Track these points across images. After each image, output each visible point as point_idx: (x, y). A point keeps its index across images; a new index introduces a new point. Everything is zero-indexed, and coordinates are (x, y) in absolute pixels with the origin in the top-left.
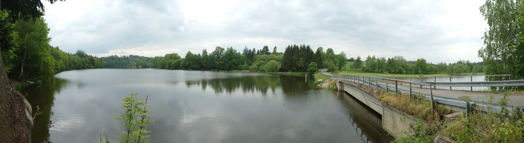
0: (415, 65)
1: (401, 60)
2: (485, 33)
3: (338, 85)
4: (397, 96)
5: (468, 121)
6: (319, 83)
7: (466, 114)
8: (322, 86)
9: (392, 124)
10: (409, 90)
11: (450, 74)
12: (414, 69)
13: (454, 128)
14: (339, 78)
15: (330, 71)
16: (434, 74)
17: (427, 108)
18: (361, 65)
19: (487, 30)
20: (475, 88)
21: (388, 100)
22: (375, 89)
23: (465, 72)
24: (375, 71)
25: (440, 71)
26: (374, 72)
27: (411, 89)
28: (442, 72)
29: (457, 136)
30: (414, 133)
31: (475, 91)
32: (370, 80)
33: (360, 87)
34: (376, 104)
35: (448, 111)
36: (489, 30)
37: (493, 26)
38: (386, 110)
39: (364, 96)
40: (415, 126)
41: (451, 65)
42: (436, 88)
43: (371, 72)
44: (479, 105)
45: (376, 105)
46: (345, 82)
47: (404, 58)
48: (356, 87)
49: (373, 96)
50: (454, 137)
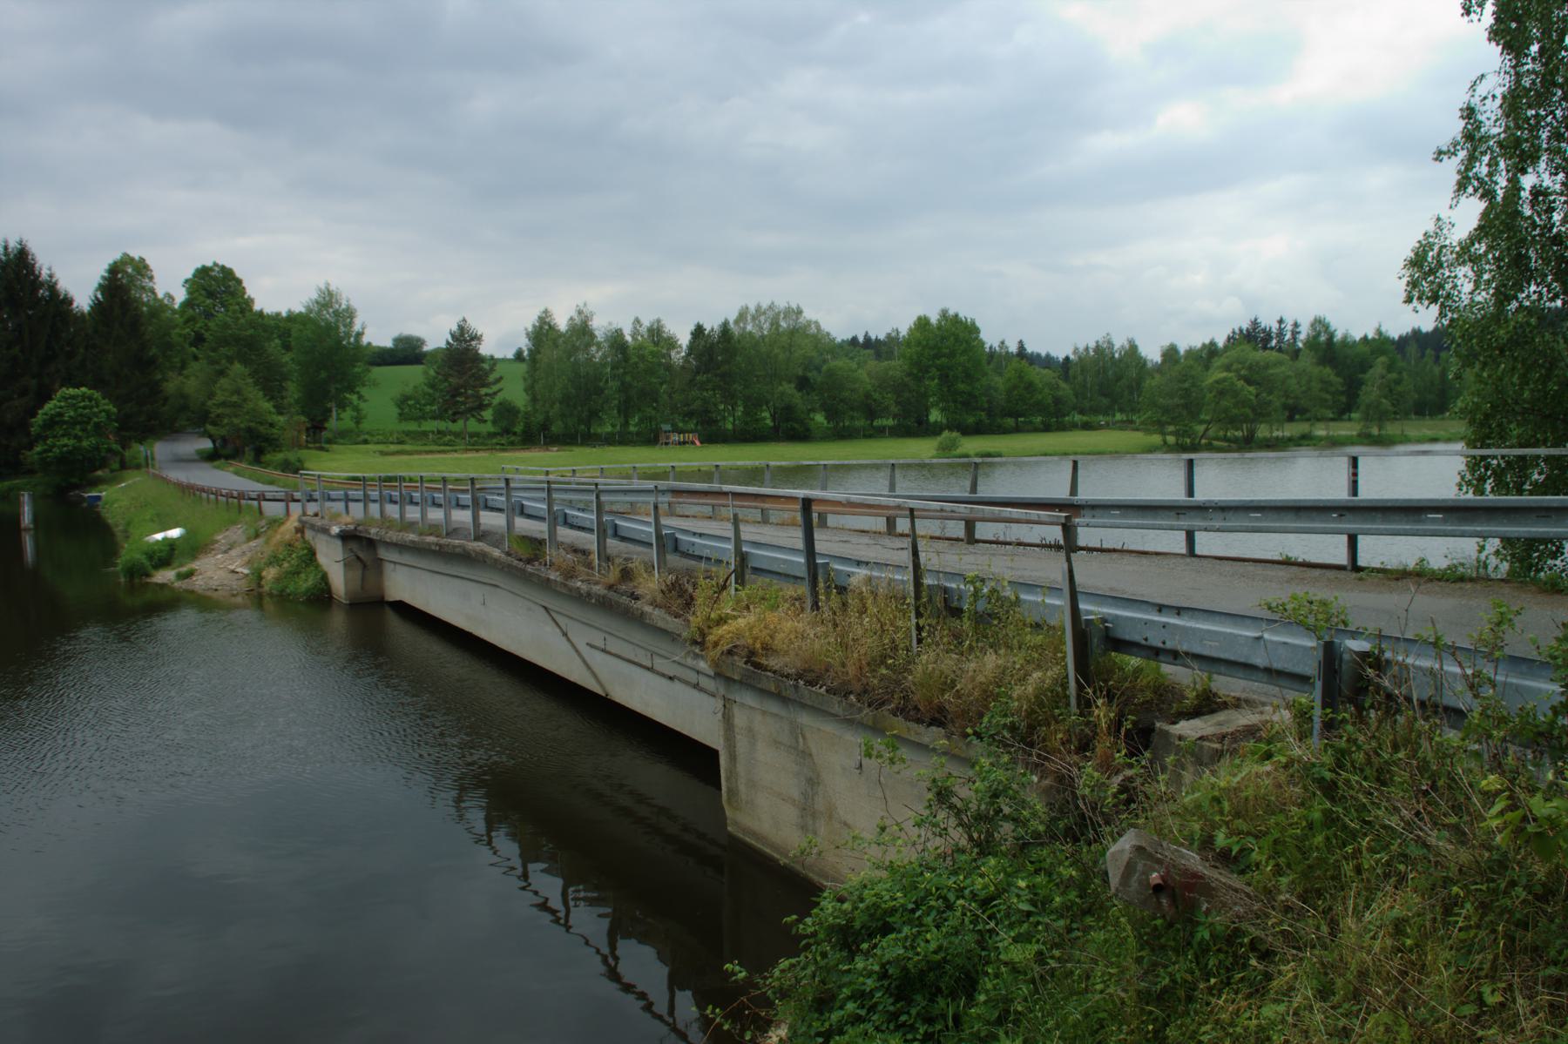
0: (896, 367)
1: (793, 332)
2: (1469, 113)
3: (332, 561)
4: (816, 606)
5: (1328, 759)
6: (167, 555)
7: (1317, 712)
8: (198, 583)
9: (795, 793)
10: (905, 557)
11: (1171, 428)
12: (889, 400)
13: (1230, 800)
14: (340, 506)
15: (228, 450)
16: (1047, 428)
17: (1037, 675)
18: (483, 391)
19: (1482, 90)
20: (1379, 549)
21: (755, 639)
22: (649, 568)
23: (1293, 412)
24: (597, 429)
25: (1095, 411)
26: (589, 439)
27: (915, 553)
28: (1106, 413)
29: (1250, 842)
30: (958, 836)
31: (1379, 571)
32: (599, 505)
33: (529, 561)
34: (663, 675)
35: (1184, 697)
36: (1499, 92)
37: (1535, 48)
38: (743, 705)
39: (554, 615)
40: (968, 793)
41: (1177, 362)
42: (1081, 542)
43: (568, 439)
44: (1409, 661)
45: (665, 682)
46: (393, 536)
47: (809, 314)
48: (496, 560)
49: (639, 620)
50: (1235, 849)
